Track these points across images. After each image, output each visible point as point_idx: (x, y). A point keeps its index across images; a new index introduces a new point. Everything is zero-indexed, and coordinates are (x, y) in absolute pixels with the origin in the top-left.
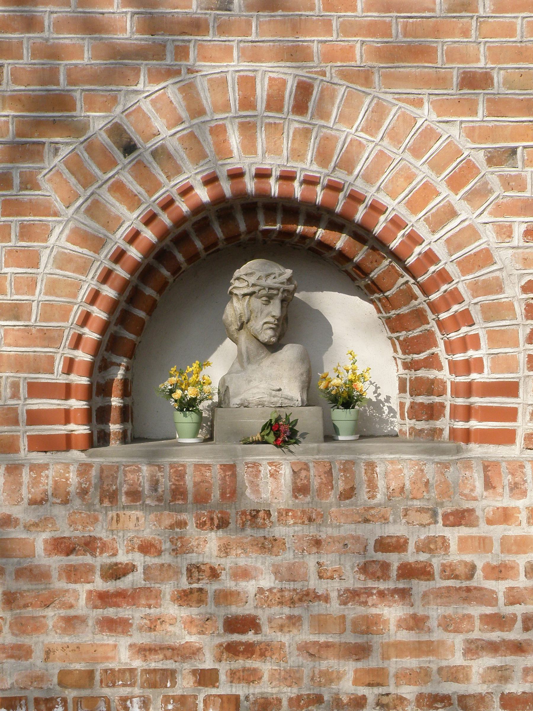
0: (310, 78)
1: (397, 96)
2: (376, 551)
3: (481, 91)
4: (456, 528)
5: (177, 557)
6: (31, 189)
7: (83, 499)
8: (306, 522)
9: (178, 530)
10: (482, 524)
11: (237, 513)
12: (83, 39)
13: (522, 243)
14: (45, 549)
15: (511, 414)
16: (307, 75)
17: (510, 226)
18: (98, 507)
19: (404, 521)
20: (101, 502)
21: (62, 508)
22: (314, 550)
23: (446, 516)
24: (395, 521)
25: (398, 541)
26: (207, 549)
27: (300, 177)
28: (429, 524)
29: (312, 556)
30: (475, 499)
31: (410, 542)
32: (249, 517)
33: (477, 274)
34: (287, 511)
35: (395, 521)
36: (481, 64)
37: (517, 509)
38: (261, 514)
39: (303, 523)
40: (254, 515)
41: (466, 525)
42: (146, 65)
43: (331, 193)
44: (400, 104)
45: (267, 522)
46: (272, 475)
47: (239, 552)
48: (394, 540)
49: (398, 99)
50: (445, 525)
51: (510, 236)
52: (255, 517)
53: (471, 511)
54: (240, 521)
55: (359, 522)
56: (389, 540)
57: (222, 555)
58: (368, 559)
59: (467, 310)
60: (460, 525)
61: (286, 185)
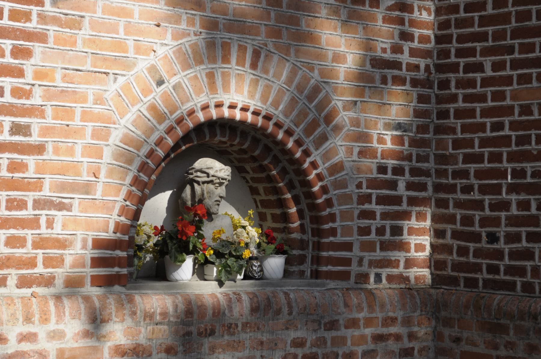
0: (259, 47)
1: (302, 64)
2: (291, 347)
3: (342, 65)
4: (330, 332)
5: (186, 356)
6: (100, 104)
7: (133, 319)
8: (256, 330)
9: (187, 337)
10: (343, 328)
11: (220, 326)
12: (134, 5)
13: (357, 159)
14: (109, 353)
15: (347, 262)
16: (258, 45)
17: (352, 148)
18: (142, 323)
19: (305, 328)
20: (145, 320)
21: (120, 324)
22: (260, 348)
23: (325, 325)
24: (301, 328)
25: (302, 341)
26: (203, 350)
27: (212, 105)
28: (317, 330)
29: (259, 352)
30: (339, 314)
31: (308, 341)
32: (226, 328)
33: (337, 176)
34: (247, 323)
35: (301, 328)
36: (342, 49)
37: (359, 320)
38: (233, 326)
39: (254, 331)
40: (230, 326)
41: (335, 330)
42: (171, 27)
43: (266, 121)
44: (304, 69)
45: (236, 331)
46: (238, 301)
47: (220, 350)
48: (300, 339)
49: (303, 66)
50: (325, 330)
51: (352, 154)
52: (229, 328)
53: (337, 321)
54: (221, 331)
55: (283, 330)
56: (298, 340)
57: (211, 353)
58: (287, 352)
59: (331, 198)
60: (332, 329)
61: (244, 113)
